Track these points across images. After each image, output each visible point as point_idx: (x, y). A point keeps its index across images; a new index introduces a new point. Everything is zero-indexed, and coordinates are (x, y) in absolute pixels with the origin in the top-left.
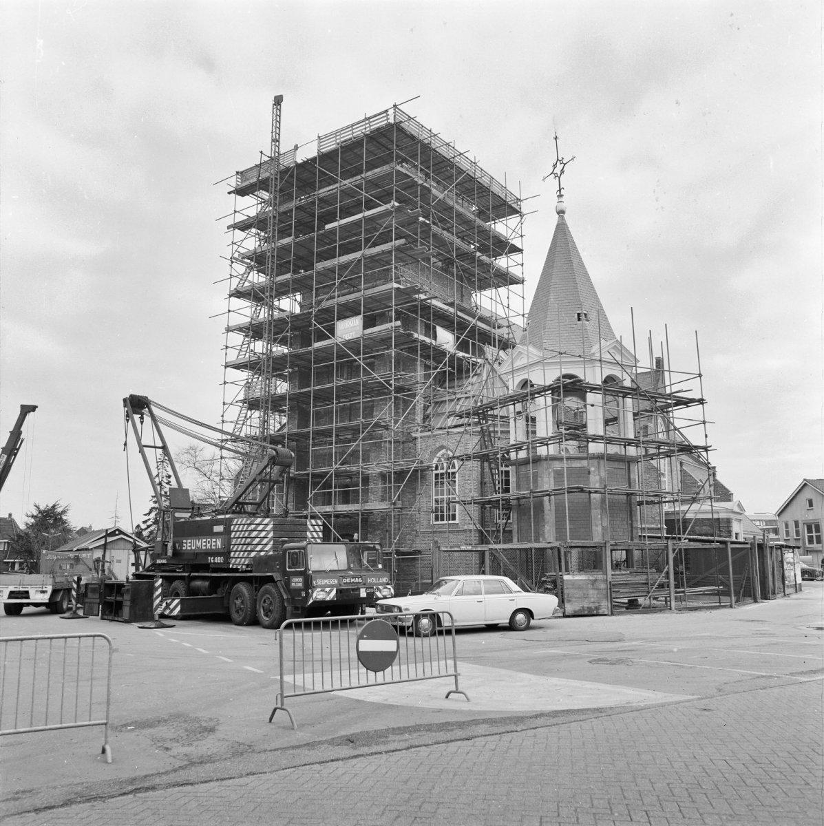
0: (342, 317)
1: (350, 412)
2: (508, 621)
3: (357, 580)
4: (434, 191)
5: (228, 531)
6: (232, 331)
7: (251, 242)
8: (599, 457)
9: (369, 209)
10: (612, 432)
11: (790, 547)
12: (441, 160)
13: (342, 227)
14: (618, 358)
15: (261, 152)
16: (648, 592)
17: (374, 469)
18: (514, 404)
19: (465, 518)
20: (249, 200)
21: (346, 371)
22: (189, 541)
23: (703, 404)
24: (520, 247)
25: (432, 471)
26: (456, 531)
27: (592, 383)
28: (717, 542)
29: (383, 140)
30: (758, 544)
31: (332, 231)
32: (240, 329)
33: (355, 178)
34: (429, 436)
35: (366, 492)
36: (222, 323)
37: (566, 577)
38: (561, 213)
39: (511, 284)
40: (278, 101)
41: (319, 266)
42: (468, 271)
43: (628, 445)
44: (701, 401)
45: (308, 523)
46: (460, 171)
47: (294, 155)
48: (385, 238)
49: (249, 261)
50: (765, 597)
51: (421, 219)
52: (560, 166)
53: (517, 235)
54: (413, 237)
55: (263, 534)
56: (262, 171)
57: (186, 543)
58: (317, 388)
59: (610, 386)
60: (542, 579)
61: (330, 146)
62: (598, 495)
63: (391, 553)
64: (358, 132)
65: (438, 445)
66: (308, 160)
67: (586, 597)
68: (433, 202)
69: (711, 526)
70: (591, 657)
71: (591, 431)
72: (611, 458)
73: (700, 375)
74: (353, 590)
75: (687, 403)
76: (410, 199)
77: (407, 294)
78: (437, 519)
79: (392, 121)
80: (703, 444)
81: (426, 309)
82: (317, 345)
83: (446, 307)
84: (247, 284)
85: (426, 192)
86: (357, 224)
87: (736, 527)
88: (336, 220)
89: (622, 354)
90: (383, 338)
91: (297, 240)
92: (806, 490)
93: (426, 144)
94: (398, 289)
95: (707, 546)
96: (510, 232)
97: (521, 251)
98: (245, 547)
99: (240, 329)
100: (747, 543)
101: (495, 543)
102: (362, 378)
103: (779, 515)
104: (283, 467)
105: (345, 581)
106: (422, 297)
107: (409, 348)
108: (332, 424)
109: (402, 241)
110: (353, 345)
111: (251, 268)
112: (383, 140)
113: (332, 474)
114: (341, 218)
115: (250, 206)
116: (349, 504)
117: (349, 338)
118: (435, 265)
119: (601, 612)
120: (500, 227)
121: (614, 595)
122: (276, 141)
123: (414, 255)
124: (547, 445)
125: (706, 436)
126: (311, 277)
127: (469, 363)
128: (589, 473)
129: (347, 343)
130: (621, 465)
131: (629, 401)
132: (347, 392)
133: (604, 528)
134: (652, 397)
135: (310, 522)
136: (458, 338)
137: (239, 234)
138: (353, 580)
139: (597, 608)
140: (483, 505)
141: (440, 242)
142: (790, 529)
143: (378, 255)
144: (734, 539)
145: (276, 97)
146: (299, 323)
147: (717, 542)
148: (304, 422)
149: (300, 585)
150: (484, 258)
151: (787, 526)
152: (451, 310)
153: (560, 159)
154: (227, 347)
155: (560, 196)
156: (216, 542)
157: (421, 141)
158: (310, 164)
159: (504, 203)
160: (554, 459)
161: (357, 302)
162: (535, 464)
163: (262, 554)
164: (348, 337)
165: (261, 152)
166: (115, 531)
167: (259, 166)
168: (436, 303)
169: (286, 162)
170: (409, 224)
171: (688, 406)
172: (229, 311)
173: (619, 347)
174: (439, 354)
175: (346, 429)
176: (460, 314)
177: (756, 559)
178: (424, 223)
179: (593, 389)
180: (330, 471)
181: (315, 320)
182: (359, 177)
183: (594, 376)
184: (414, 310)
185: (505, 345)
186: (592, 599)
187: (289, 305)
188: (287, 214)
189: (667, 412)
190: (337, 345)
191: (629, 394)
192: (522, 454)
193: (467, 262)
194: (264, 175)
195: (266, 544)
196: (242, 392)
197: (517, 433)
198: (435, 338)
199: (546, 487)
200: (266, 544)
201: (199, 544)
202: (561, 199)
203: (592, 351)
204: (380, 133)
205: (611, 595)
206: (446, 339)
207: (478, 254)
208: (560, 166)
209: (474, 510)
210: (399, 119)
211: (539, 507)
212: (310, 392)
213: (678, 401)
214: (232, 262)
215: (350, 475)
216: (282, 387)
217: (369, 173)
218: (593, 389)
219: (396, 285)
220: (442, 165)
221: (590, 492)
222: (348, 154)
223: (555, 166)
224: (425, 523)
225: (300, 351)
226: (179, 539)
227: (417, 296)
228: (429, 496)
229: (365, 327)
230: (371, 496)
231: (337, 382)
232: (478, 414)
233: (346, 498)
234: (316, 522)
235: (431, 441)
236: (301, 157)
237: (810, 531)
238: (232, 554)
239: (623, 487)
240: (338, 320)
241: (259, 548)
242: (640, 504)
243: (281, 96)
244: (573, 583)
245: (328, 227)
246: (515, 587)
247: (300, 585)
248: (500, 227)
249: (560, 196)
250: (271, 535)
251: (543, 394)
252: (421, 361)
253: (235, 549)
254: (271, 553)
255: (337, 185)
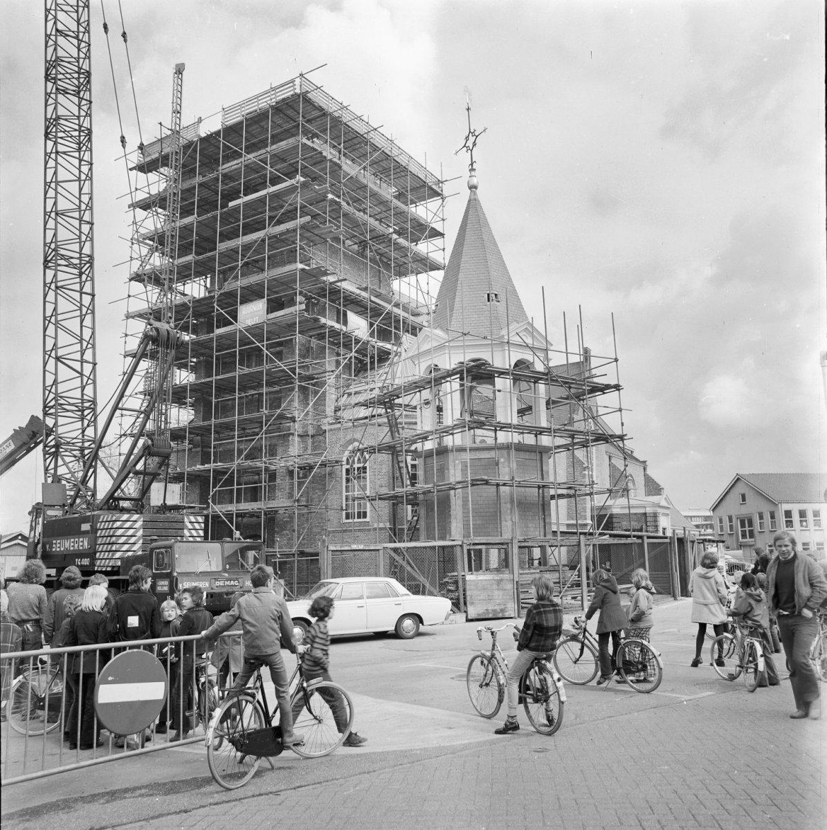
0: (245, 300)
1: (256, 403)
2: (393, 628)
3: (232, 583)
4: (345, 167)
5: (94, 530)
6: (133, 317)
7: (152, 222)
8: (507, 447)
9: (273, 184)
10: (528, 420)
11: (714, 541)
12: (354, 136)
13: (246, 205)
14: (529, 341)
15: (160, 124)
16: (560, 593)
17: (279, 464)
18: (420, 391)
19: (378, 516)
20: (153, 176)
21: (254, 358)
22: (81, 539)
23: (619, 390)
24: (442, 231)
25: (342, 465)
26: (365, 529)
27: (500, 366)
28: (634, 536)
29: (290, 112)
30: (678, 539)
31: (236, 209)
32: (141, 316)
33: (260, 152)
34: (339, 429)
35: (272, 489)
36: (122, 309)
37: (469, 577)
38: (473, 188)
39: (432, 269)
40: (179, 70)
41: (222, 246)
42: (385, 255)
43: (540, 434)
44: (617, 387)
45: (186, 520)
46: (375, 148)
47: (196, 130)
48: (290, 215)
49: (151, 243)
50: (87, 745)
51: (330, 196)
52: (472, 139)
53: (439, 219)
54: (322, 217)
55: (130, 532)
56: (164, 145)
57: (56, 544)
58: (219, 377)
59: (522, 373)
60: (445, 580)
61: (234, 119)
62: (507, 489)
63: (294, 555)
64: (264, 104)
65: (348, 437)
66: (211, 134)
67: (490, 599)
68: (344, 179)
69: (638, 521)
70: (459, 671)
71: (501, 418)
72: (520, 448)
73: (616, 360)
74: (227, 594)
75: (604, 389)
76: (321, 176)
77: (314, 276)
78: (347, 517)
79: (298, 91)
80: (618, 432)
81: (334, 293)
82: (219, 331)
83: (358, 291)
84: (148, 267)
85: (336, 168)
86: (262, 200)
87: (664, 522)
88: (240, 197)
89: (533, 337)
90: (289, 322)
91: (200, 219)
92: (739, 485)
93: (336, 117)
94: (303, 270)
95: (623, 541)
96: (430, 216)
97: (442, 235)
98: (110, 546)
99: (141, 316)
100: (666, 538)
101: (399, 542)
102: (266, 367)
103: (713, 510)
104: (161, 459)
105: (218, 583)
106: (331, 279)
107: (318, 335)
108: (234, 415)
109: (308, 218)
110: (256, 330)
111: (152, 251)
112: (290, 112)
113: (233, 472)
114: (245, 195)
115: (156, 183)
116: (256, 501)
117: (253, 323)
118: (350, 248)
119: (507, 615)
120: (423, 211)
121: (522, 596)
122: (177, 112)
123: (322, 234)
124: (452, 434)
125: (622, 424)
126: (213, 259)
127: (374, 347)
128: (497, 464)
129: (249, 329)
130: (533, 456)
131: (542, 387)
132: (250, 382)
133: (514, 523)
134: (566, 383)
135: (188, 518)
136: (371, 325)
137: (141, 214)
138: (228, 583)
139: (502, 611)
140: (396, 501)
141: (355, 224)
142: (724, 524)
143: (282, 234)
144: (661, 534)
145: (177, 65)
146: (203, 309)
147: (634, 536)
148: (207, 417)
149: (166, 588)
150: (401, 241)
151: (721, 521)
152: (364, 294)
153: (472, 131)
154: (126, 335)
155: (472, 170)
156: (83, 542)
157: (330, 114)
158: (215, 138)
159: (424, 184)
160: (461, 449)
161: (261, 285)
162: (441, 456)
163: (130, 554)
164: (250, 322)
165: (160, 124)
166: (18, 535)
167: (161, 140)
168: (345, 285)
169: (190, 136)
170: (317, 202)
171: (604, 393)
172: (129, 296)
173: (531, 330)
174: (347, 341)
175: (251, 421)
176: (373, 299)
177: (675, 555)
178: (333, 201)
179: (502, 373)
180: (228, 469)
181: (218, 305)
182: (263, 151)
183: (501, 360)
184: (322, 293)
185: (414, 330)
186: (498, 601)
187: (196, 289)
188: (191, 190)
189: (583, 400)
190: (240, 331)
191: (541, 379)
192: (429, 445)
193: (384, 245)
194: (166, 150)
195: (134, 543)
196: (142, 383)
197: (426, 421)
198: (345, 323)
199: (452, 480)
200: (134, 543)
201: (67, 545)
202: (473, 173)
203: (502, 334)
204: (287, 104)
205: (518, 596)
206: (358, 325)
207: (395, 236)
208: (472, 139)
209: (384, 507)
210: (305, 88)
211: (445, 503)
212: (212, 382)
213: (593, 387)
214: (133, 244)
215: (258, 472)
216: (183, 377)
217: (274, 147)
218: (502, 373)
219: (300, 266)
220: (355, 141)
221: (498, 485)
222: (254, 127)
223: (467, 138)
224: (335, 521)
225: (203, 337)
226: (50, 539)
227: (325, 278)
228: (338, 494)
229: (270, 310)
230: (278, 493)
231: (240, 371)
232: (385, 403)
233: (254, 495)
234: (196, 519)
235: (341, 434)
236: (204, 131)
237: (743, 525)
238: (98, 555)
239: (534, 478)
240: (241, 303)
241: (125, 547)
242: (553, 497)
243: (183, 65)
244: (476, 583)
245: (231, 204)
246: (401, 589)
247: (166, 588)
248: (423, 211)
249: (472, 170)
250: (140, 533)
251: (449, 379)
252: (329, 348)
253: (100, 550)
254: (140, 553)
255: (242, 160)
